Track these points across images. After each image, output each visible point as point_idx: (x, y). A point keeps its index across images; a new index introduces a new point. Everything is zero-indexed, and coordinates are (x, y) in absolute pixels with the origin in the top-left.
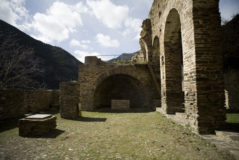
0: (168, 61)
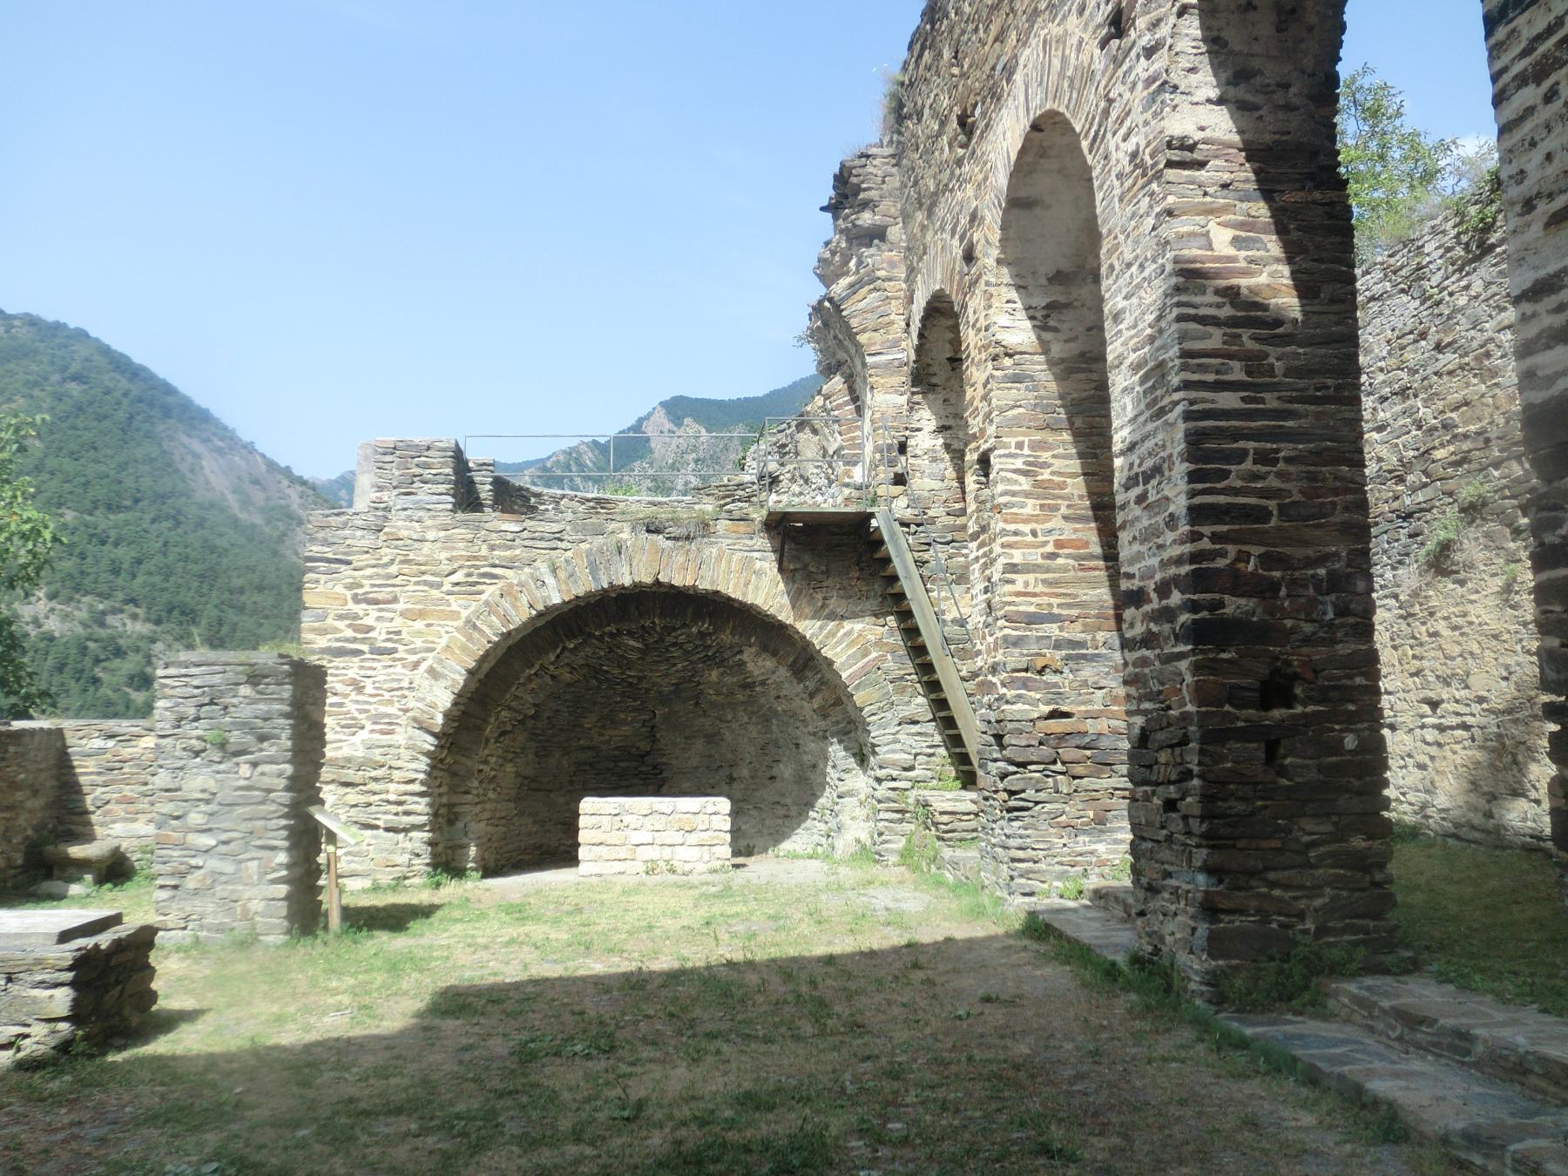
0: (1027, 495)
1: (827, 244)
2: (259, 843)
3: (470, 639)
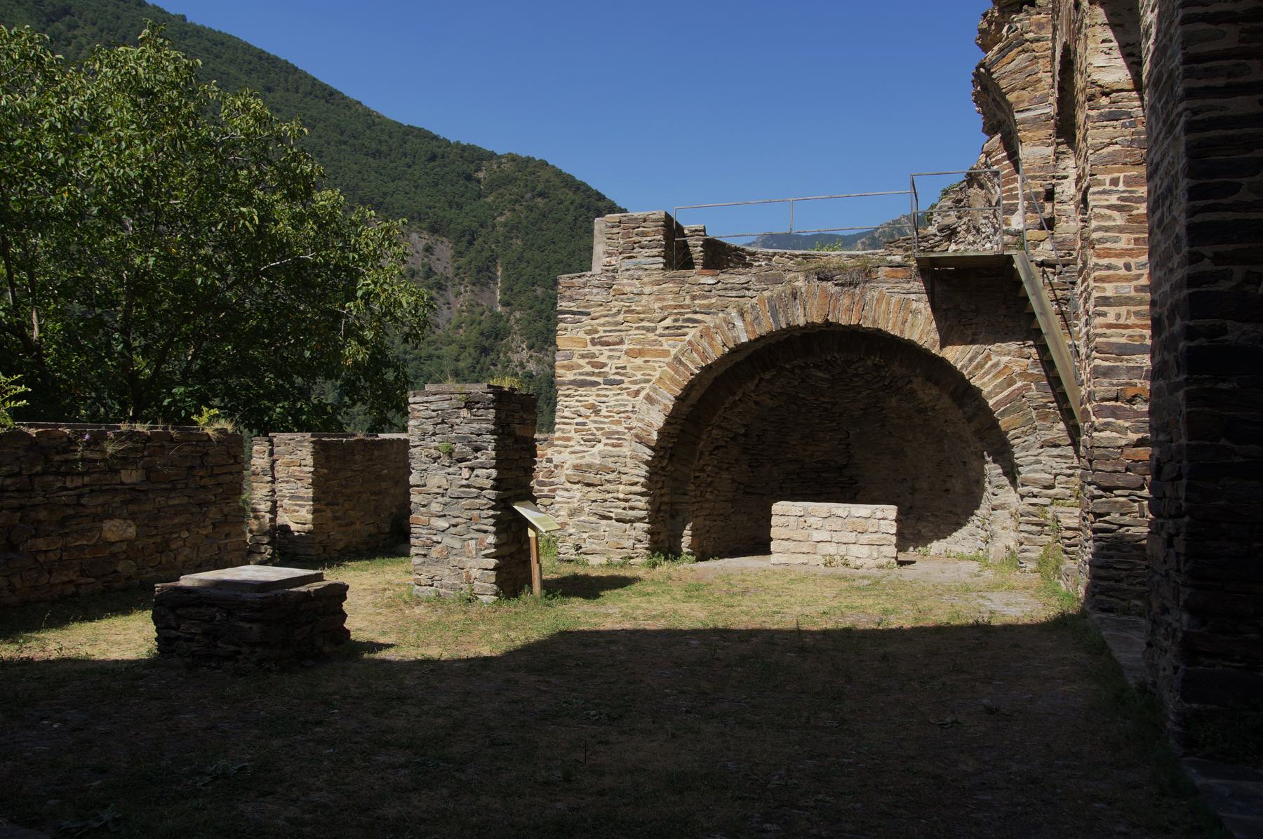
0: (1121, 230)
1: (985, 15)
2: (476, 527)
3: (676, 371)
